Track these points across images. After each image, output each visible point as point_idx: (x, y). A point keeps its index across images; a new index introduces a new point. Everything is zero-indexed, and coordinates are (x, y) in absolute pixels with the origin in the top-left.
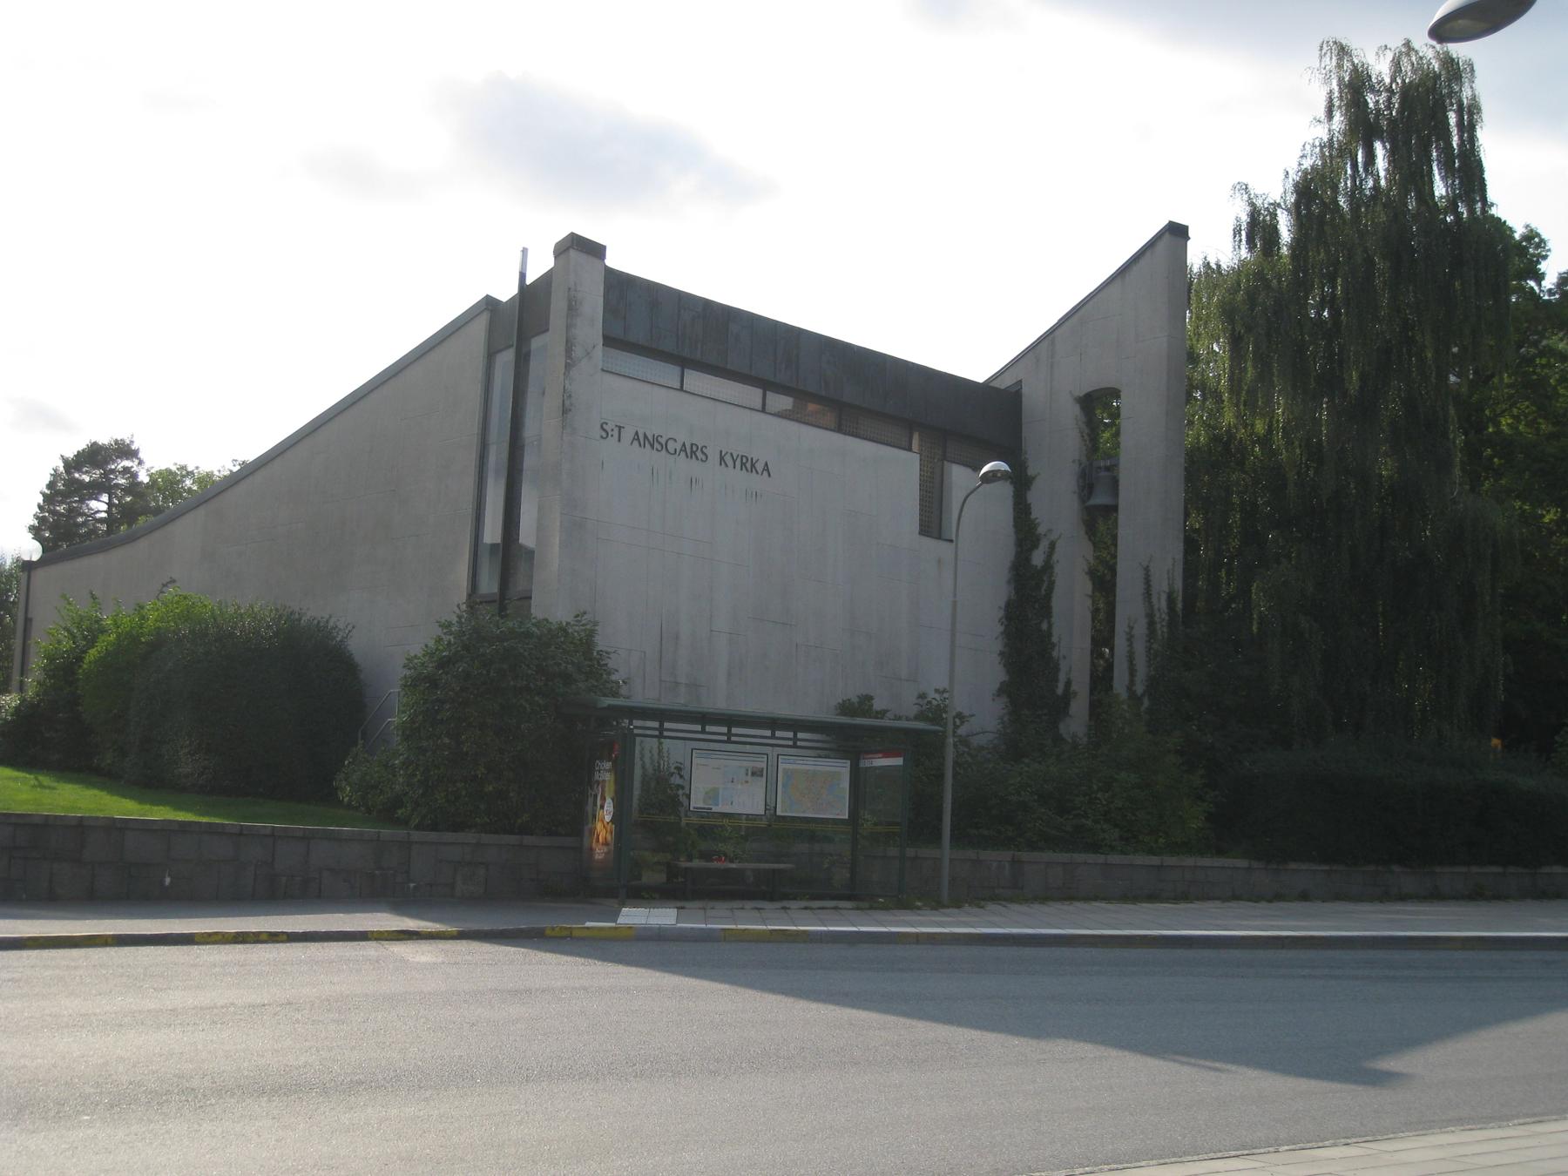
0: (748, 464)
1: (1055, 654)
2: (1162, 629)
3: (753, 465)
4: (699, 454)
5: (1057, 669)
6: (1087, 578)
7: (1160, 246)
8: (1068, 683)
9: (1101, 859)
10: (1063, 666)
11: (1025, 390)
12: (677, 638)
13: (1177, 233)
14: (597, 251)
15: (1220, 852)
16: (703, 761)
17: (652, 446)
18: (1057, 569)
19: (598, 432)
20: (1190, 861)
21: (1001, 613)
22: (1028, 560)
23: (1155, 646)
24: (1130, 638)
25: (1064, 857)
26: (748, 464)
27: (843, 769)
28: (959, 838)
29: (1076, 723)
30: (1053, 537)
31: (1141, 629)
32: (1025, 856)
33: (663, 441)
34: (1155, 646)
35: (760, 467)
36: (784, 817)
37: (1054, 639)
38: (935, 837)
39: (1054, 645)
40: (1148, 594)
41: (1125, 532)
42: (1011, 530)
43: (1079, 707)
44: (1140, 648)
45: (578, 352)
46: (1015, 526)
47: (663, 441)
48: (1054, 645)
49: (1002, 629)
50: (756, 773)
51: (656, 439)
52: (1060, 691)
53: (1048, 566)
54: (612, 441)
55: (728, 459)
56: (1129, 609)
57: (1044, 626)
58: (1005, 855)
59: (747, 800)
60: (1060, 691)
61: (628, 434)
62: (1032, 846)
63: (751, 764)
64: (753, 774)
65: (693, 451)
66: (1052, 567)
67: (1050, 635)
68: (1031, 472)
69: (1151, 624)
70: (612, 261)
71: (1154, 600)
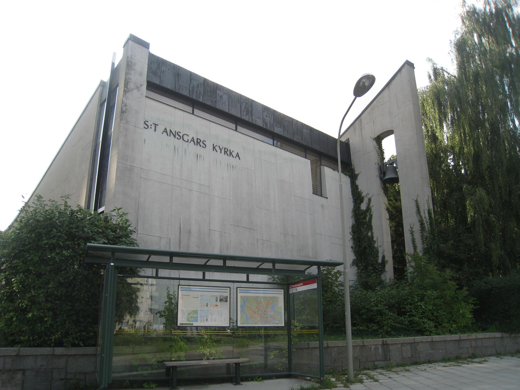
0: (228, 152)
1: (376, 245)
2: (427, 226)
3: (231, 153)
4: (201, 143)
5: (377, 251)
6: (386, 212)
7: (404, 70)
8: (384, 257)
9: (429, 338)
10: (380, 250)
11: (351, 142)
12: (190, 232)
13: (409, 65)
14: (146, 45)
15: (484, 330)
16: (185, 293)
17: (175, 136)
18: (373, 209)
19: (142, 125)
20: (474, 336)
21: (351, 230)
22: (359, 207)
23: (425, 234)
24: (412, 233)
25: (410, 339)
26: (228, 152)
27: (279, 295)
28: (356, 334)
29: (389, 274)
30: (369, 196)
31: (417, 227)
32: (389, 340)
33: (181, 135)
34: (425, 234)
35: (234, 154)
36: (242, 327)
37: (375, 239)
38: (340, 331)
39: (375, 242)
40: (418, 211)
41: (403, 186)
42: (351, 196)
43: (389, 267)
44: (418, 236)
45: (131, 86)
46: (352, 195)
47: (181, 135)
48: (375, 242)
49: (351, 237)
50: (223, 300)
51: (178, 133)
52: (380, 261)
53: (369, 209)
54: (151, 131)
55: (217, 148)
56: (410, 220)
57: (370, 234)
58: (379, 341)
59: (218, 318)
60: (380, 261)
61: (160, 129)
62: (388, 334)
63: (218, 294)
64: (221, 300)
65: (198, 142)
66: (370, 209)
67: (373, 237)
68: (356, 173)
69: (422, 224)
70: (154, 50)
71: (422, 214)
